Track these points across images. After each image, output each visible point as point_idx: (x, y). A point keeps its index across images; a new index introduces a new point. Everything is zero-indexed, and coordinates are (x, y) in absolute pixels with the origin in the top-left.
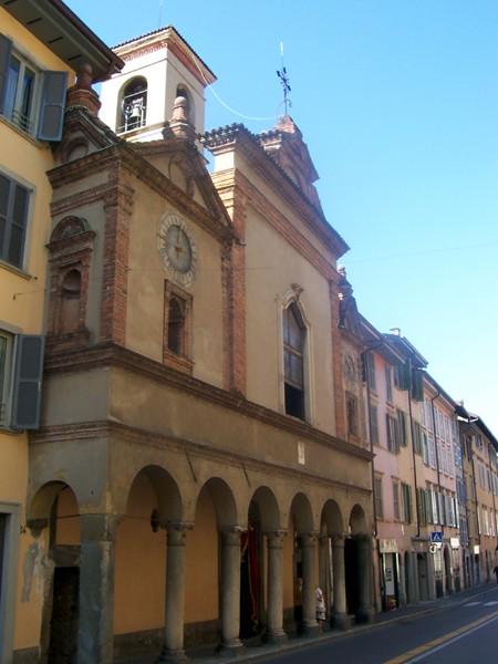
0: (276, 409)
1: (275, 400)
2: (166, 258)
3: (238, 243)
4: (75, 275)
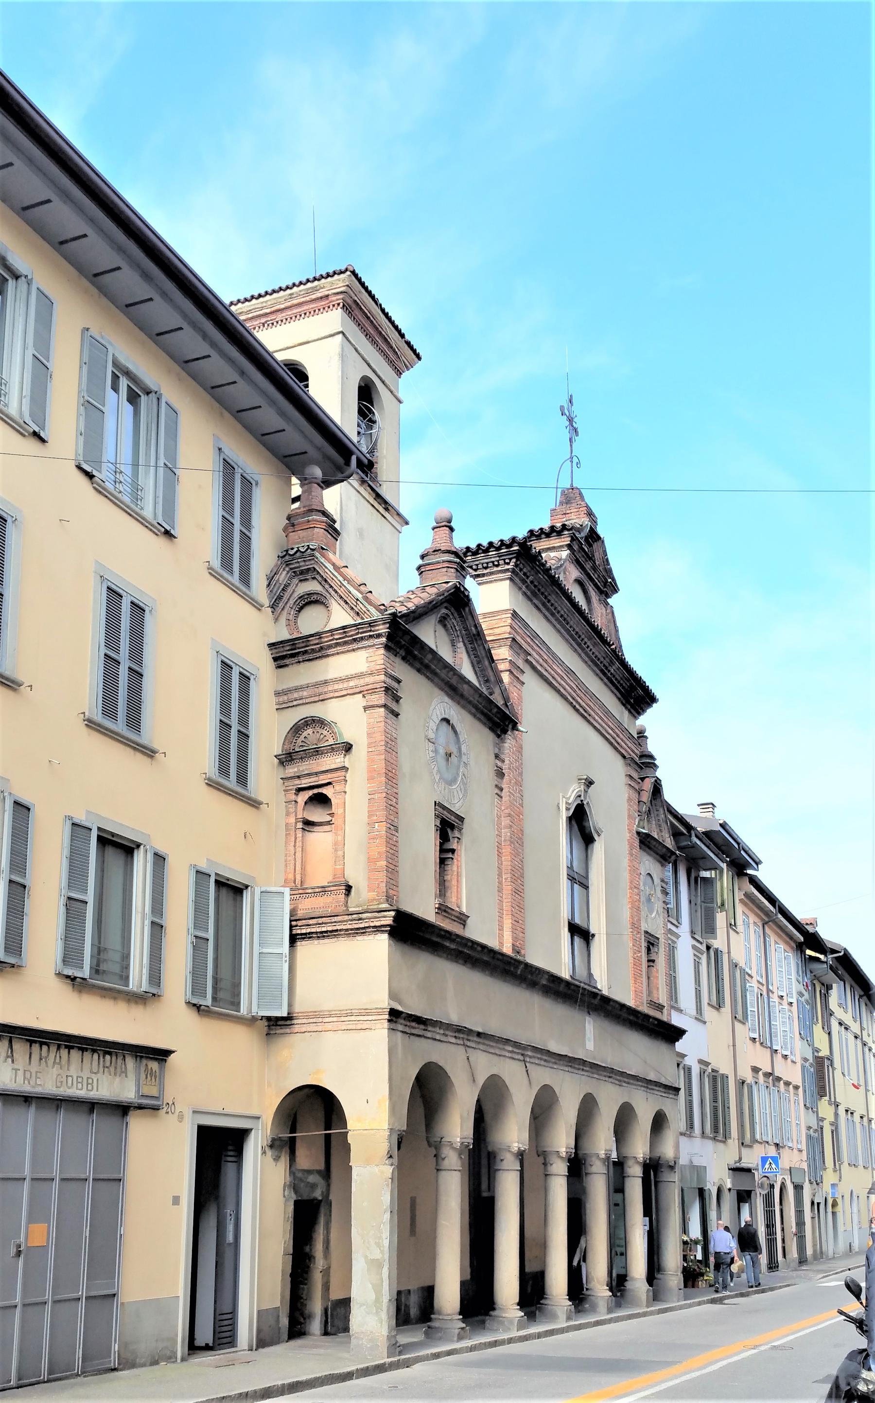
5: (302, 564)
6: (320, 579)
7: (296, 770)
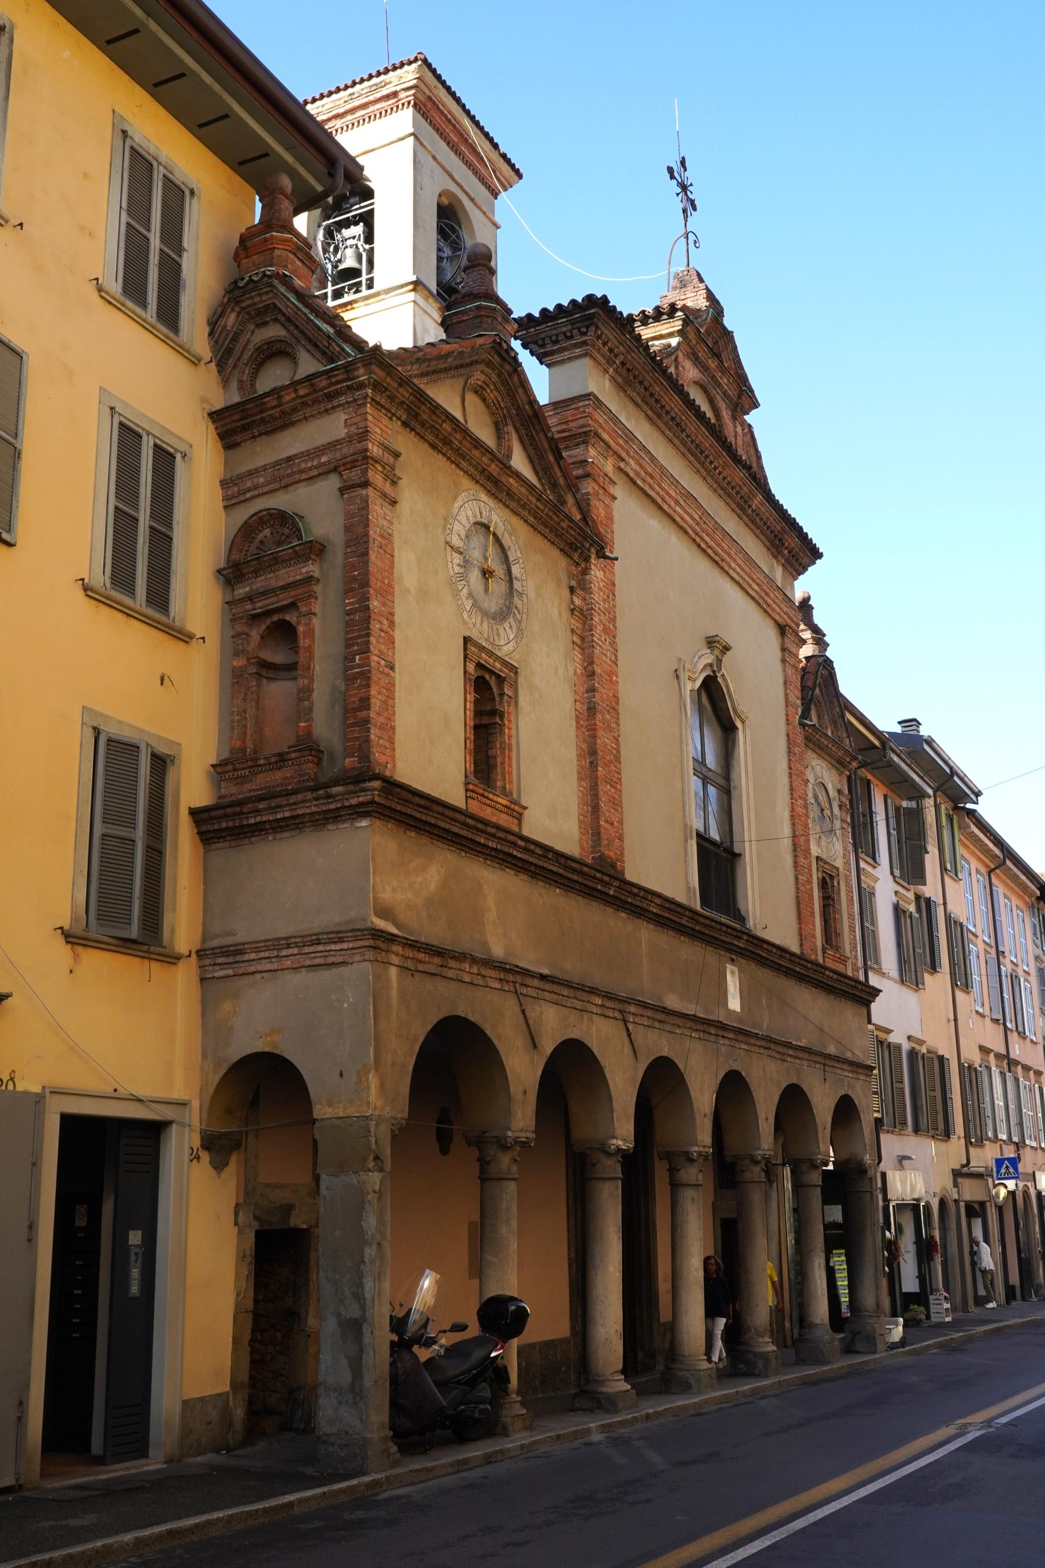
0: (681, 898)
1: (675, 877)
2: (465, 591)
3: (601, 555)
4: (284, 632)
5: (257, 299)
6: (282, 319)
7: (248, 589)
